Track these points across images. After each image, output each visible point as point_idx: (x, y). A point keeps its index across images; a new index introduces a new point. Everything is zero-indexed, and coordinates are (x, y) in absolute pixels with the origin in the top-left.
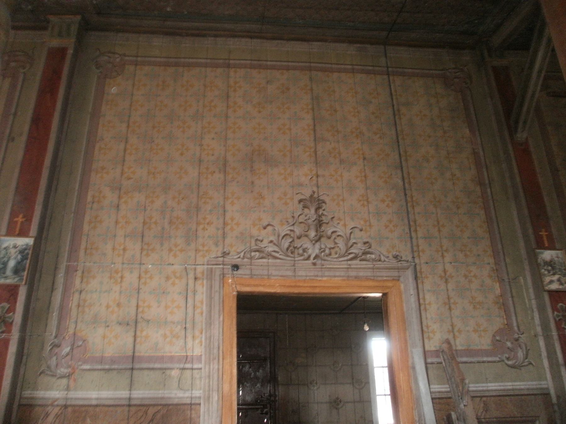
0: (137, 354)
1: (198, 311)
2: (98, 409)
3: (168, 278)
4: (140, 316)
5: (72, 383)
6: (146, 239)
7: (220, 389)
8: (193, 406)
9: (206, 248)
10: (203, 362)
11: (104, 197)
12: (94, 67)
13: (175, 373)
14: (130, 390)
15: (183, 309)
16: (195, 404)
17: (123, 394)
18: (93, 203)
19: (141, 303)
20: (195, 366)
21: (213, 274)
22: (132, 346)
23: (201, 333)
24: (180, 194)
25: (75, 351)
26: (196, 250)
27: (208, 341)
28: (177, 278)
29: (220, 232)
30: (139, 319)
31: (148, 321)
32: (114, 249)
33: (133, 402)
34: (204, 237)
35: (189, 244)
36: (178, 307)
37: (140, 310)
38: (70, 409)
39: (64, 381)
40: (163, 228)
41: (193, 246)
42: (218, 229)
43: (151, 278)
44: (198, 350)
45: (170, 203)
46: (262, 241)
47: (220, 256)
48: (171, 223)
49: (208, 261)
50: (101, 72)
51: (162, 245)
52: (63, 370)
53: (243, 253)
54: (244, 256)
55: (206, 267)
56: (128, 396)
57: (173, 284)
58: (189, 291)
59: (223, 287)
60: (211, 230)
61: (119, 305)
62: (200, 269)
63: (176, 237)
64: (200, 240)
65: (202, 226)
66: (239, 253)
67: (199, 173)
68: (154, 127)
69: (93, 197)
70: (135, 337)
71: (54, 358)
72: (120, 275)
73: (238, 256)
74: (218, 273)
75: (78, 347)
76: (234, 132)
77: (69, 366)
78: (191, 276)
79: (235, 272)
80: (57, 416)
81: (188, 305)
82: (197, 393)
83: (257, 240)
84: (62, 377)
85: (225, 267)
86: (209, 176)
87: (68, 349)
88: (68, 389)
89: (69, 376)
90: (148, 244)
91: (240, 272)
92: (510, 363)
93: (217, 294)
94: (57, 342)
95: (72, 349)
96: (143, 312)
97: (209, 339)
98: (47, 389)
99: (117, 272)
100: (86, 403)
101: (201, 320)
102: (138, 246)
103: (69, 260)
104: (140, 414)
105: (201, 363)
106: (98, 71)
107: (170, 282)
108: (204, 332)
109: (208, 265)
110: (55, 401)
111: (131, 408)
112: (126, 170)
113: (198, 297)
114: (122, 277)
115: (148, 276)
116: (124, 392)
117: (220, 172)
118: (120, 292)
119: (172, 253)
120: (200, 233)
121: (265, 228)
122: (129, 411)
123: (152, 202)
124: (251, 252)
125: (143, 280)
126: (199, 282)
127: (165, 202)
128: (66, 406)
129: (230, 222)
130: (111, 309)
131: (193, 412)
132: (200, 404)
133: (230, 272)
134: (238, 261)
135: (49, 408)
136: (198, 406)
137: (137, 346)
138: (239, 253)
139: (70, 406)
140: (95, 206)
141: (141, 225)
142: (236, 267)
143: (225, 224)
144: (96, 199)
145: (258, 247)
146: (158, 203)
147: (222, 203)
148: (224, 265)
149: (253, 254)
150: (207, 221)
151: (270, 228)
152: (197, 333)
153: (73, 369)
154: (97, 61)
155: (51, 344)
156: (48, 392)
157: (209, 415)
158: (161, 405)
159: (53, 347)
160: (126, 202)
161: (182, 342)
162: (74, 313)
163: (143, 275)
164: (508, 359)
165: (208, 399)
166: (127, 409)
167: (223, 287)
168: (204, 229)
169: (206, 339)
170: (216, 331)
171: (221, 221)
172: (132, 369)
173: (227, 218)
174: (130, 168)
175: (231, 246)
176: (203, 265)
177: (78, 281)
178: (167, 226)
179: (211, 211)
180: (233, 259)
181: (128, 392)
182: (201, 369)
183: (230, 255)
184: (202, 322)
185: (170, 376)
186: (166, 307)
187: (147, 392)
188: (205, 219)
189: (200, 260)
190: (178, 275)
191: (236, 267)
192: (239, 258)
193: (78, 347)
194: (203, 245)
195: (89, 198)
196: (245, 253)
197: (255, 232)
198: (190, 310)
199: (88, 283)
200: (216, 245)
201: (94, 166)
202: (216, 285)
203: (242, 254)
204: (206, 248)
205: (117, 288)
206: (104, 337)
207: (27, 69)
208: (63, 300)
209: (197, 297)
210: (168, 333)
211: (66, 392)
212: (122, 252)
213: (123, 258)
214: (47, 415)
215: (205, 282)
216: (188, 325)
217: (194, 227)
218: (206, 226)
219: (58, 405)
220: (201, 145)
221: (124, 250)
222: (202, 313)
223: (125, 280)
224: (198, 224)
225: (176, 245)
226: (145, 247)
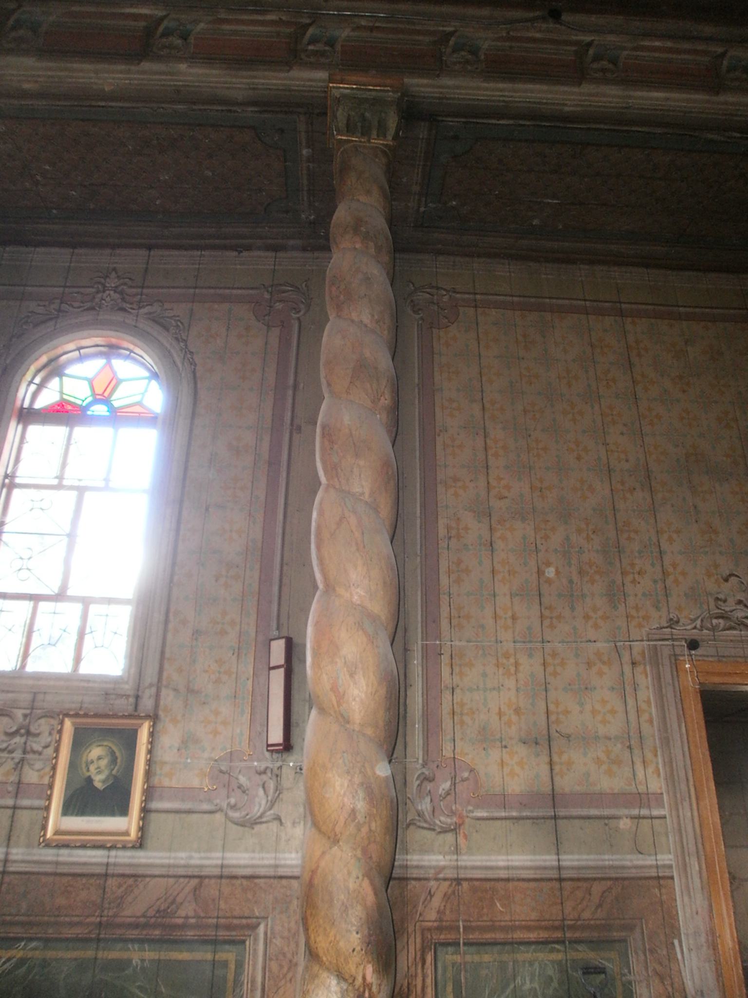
1: (645, 717)
2: (510, 885)
3: (589, 664)
4: (553, 727)
6: (546, 600)
7: (701, 853)
8: (662, 880)
9: (641, 614)
10: (666, 806)
11: (466, 529)
12: (409, 310)
13: (624, 824)
14: (558, 854)
16: (664, 878)
18: (450, 538)
19: (552, 707)
21: (659, 654)
22: (548, 779)
23: (656, 755)
24: (587, 525)
25: (459, 787)
26: (627, 617)
27: (668, 770)
28: (604, 663)
29: (660, 585)
30: (554, 734)
31: (568, 737)
32: (496, 617)
33: (565, 874)
34: (636, 595)
35: (615, 607)
36: (613, 712)
37: (553, 718)
38: (465, 885)
39: (450, 837)
40: (571, 582)
41: (621, 608)
42: (655, 581)
43: (563, 664)
46: (725, 601)
47: (666, 625)
48: (581, 572)
49: (648, 634)
50: (422, 319)
51: (573, 609)
52: (443, 820)
53: (700, 619)
54: (701, 627)
55: (645, 643)
56: (556, 863)
57: (600, 674)
58: (626, 686)
59: (678, 676)
61: (517, 711)
62: (637, 646)
64: (631, 600)
65: (630, 578)
67: (612, 490)
68: (525, 411)
69: (448, 528)
70: (551, 763)
71: (428, 799)
72: (512, 660)
73: (693, 625)
74: (666, 652)
75: (463, 780)
77: (453, 813)
78: (626, 658)
79: (693, 652)
80: (446, 897)
81: (629, 708)
82: (666, 858)
83: (717, 599)
84: (444, 831)
85: (675, 643)
86: (628, 495)
87: (447, 785)
88: (457, 851)
89: (455, 830)
90: (550, 608)
91: (699, 651)
93: (670, 688)
94: (427, 773)
95: (454, 784)
96: (558, 721)
97: (670, 763)
98: (423, 851)
99: (507, 656)
100: (490, 874)
101: (651, 732)
102: (535, 611)
103: (425, 637)
104: (579, 894)
105: (663, 807)
106: (417, 317)
108: (659, 753)
109: (648, 641)
110: (439, 873)
113: (642, 695)
114: (517, 665)
115: (557, 661)
116: (548, 857)
118: (517, 690)
119: (590, 623)
121: (726, 580)
122: (561, 889)
123: (546, 537)
124: (711, 618)
125: (550, 669)
126: (639, 669)
127: (567, 538)
128: (458, 881)
129: (671, 570)
130: (505, 719)
131: (663, 891)
132: (672, 878)
133: (686, 651)
134: (695, 634)
135: (432, 883)
136: (670, 881)
137: (557, 779)
139: (466, 879)
141: (535, 576)
142: (693, 645)
143: (665, 573)
144: (453, 533)
145: (720, 611)
147: (654, 539)
148: (673, 640)
149: (715, 621)
150: (637, 568)
151: (733, 579)
153: (461, 817)
154: (412, 301)
155: (419, 776)
156: (426, 857)
157: (690, 897)
158: (610, 879)
159: (422, 782)
160: (503, 538)
163: (549, 660)
165: (684, 868)
166: (556, 885)
167: (678, 676)
168: (634, 581)
171: (658, 568)
172: (555, 818)
173: (667, 562)
174: (499, 479)
175: (679, 608)
176: (642, 640)
177: (445, 671)
178: (575, 578)
179: (640, 552)
180: (687, 630)
181: (555, 857)
182: (665, 817)
183: (681, 624)
184: (653, 736)
185: (617, 829)
186: (594, 712)
187: (585, 857)
190: (605, 659)
191: (693, 645)
192: (695, 628)
193: (463, 780)
194: (637, 608)
195: (442, 532)
196: (702, 621)
197: (710, 586)
198: (632, 716)
199: (461, 674)
200: (658, 608)
201: (440, 476)
202: (666, 671)
203: (698, 622)
204: (641, 614)
206: (502, 763)
207: (302, 313)
209: (639, 693)
211: (455, 857)
212: (509, 622)
213: (514, 632)
214: (431, 895)
215: (648, 668)
216: (633, 742)
217: (618, 578)
218: (636, 576)
219: (445, 879)
220: (606, 444)
221: (514, 618)
222: (651, 721)
223: (521, 668)
224: (624, 573)
225: (595, 609)
226: (547, 613)
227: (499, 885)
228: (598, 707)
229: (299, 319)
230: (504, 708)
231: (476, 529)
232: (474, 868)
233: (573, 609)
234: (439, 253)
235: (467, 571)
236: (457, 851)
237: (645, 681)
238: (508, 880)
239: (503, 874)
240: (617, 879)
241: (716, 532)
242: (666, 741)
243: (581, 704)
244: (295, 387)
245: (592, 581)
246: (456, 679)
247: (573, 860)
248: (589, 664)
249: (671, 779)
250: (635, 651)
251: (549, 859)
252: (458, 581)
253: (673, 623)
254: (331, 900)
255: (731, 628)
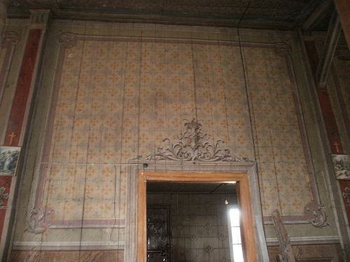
1: (122, 192)
2: (60, 253)
3: (104, 172)
4: (86, 195)
6: (90, 148)
8: (119, 251)
19: (87, 187)
29: (136, 143)
35: (117, 151)
38: (43, 253)
40: (101, 141)
41: (119, 151)
48: (105, 137)
51: (100, 151)
52: (39, 229)
64: (124, 149)
69: (58, 122)
70: (83, 208)
78: (118, 170)
82: (122, 243)
88: (42, 240)
93: (134, 182)
95: (44, 216)
96: (88, 193)
101: (124, 198)
103: (42, 161)
126: (123, 175)
127: (102, 125)
128: (41, 251)
134: (147, 162)
137: (85, 214)
142: (146, 165)
147: (137, 125)
158: (98, 250)
165: (129, 247)
168: (126, 142)
171: (137, 136)
177: (48, 173)
178: (103, 139)
179: (130, 130)
191: (146, 165)
194: (126, 152)
195: (55, 123)
199: (54, 175)
200: (134, 151)
201: (58, 103)
214: (29, 256)
227: (57, 252)
228: (105, 188)
229: (15, 45)
230: (68, 188)
231: (68, 122)
232: (48, 246)
233: (100, 151)
234: (73, 19)
235: (62, 137)
236: (42, 240)
237: (125, 179)
238: (60, 251)
239: (58, 249)
240: (101, 250)
241: (163, 123)
242: (130, 199)
243: (98, 187)
244: (9, 71)
245: (108, 158)
246: (52, 176)
247: (86, 243)
248: (104, 172)
249: (129, 215)
250: (122, 167)
251: (77, 243)
252: (59, 140)
253: (139, 157)
254: (335, 19)
255: (162, 159)
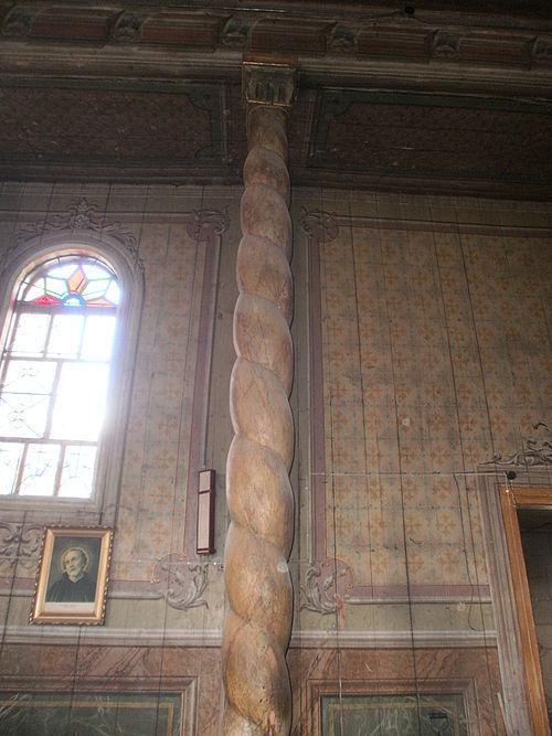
0: (411, 583)
1: (476, 529)
2: (376, 653)
3: (435, 490)
4: (408, 539)
5: (340, 620)
8: (488, 649)
13: (461, 608)
15: (458, 527)
17: (405, 634)
20: (483, 600)
22: (404, 575)
33: (417, 645)
37: (408, 529)
39: (332, 618)
41: (459, 448)
42: (483, 429)
44: (484, 579)
45: (423, 396)
57: (443, 497)
60: (477, 429)
63: (438, 439)
64: (466, 443)
65: (465, 426)
66: (511, 458)
69: (331, 389)
75: (342, 575)
76: (481, 313)
77: (334, 600)
78: (462, 483)
82: (491, 633)
89: (336, 612)
91: (516, 480)
92: (174, 601)
93: (495, 507)
97: (494, 563)
99: (374, 484)
103: (314, 468)
105: (92, 598)
107: (439, 494)
111: (417, 652)
112: (364, 356)
114: (381, 490)
117: (502, 358)
118: (382, 509)
120: (464, 434)
123: (404, 397)
128: (338, 650)
129: (495, 420)
132: (496, 647)
138: (511, 458)
140: (334, 400)
141: (395, 424)
142: (512, 476)
144: (334, 393)
146: (410, 398)
149: (527, 458)
152: (479, 557)
158: (451, 648)
160: (371, 396)
161: (463, 567)
162: (330, 534)
164: (173, 595)
168: (468, 429)
169: (490, 563)
170: (500, 554)
172: (410, 603)
181: (409, 632)
188: (467, 417)
189: (469, 468)
191: (512, 476)
195: (326, 392)
197: (524, 432)
198: (467, 529)
199: (340, 497)
202: (492, 497)
203: (516, 458)
205: (376, 504)
208: (314, 519)
210: (445, 558)
212: (376, 459)
220: (447, 327)
